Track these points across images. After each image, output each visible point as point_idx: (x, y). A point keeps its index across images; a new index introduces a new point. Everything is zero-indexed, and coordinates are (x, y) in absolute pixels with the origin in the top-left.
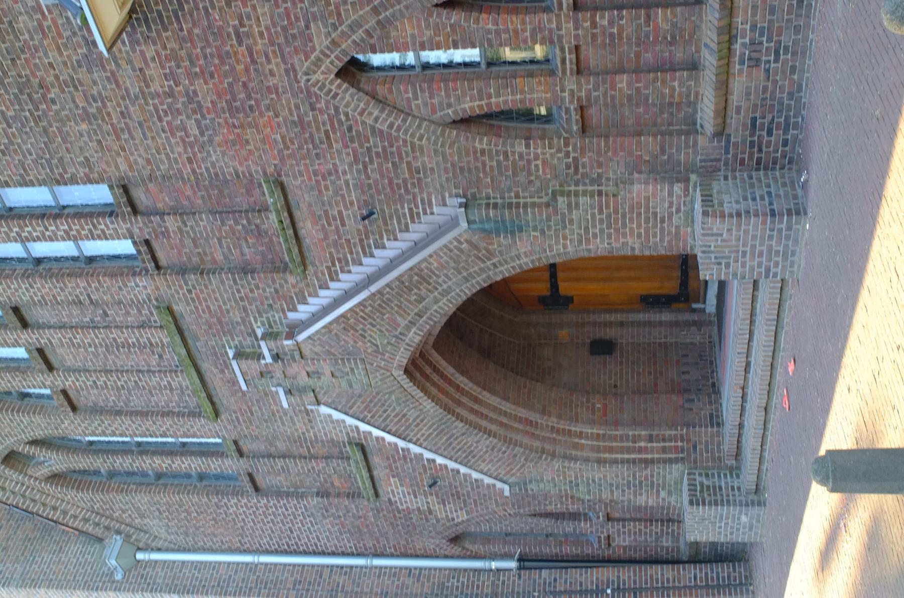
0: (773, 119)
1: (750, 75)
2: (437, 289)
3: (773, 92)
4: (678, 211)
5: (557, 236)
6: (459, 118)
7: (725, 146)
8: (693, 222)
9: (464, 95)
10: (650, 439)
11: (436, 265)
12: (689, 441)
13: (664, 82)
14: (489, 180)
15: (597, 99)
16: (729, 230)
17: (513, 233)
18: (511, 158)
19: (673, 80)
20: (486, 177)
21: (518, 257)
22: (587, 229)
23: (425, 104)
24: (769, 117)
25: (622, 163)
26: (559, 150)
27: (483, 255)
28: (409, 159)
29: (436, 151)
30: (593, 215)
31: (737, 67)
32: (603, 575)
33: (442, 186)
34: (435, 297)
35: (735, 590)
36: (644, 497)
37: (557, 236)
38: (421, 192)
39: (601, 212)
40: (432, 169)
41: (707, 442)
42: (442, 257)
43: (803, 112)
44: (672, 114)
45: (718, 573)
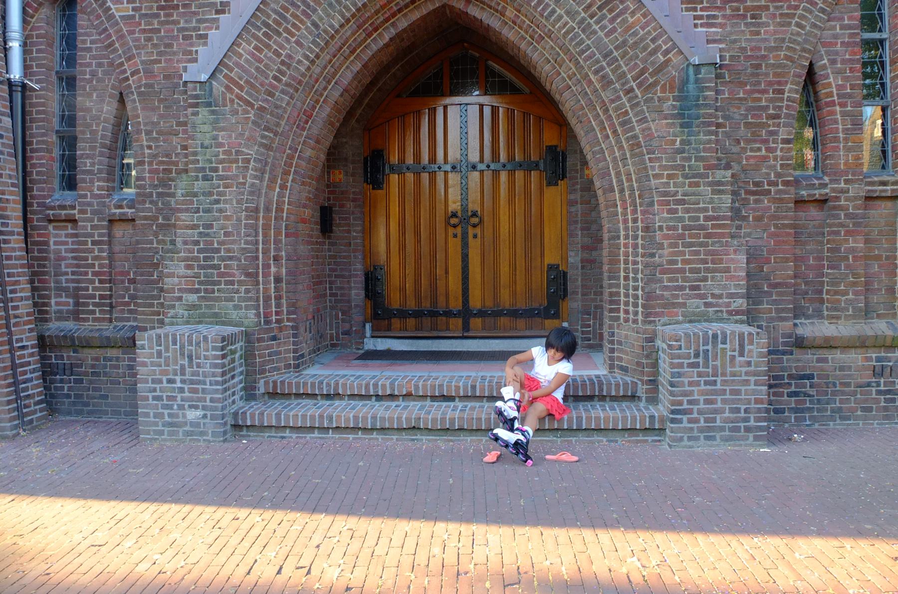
0: (809, 396)
1: (864, 368)
2: (592, 17)
3: (843, 393)
4: (707, 305)
5: (673, 168)
6: (816, 70)
7: (778, 351)
8: (690, 322)
9: (845, 79)
10: (278, 280)
11: (631, 20)
12: (281, 329)
13: (854, 284)
14: (741, 95)
15: (837, 217)
16: (749, 364)
17: (681, 116)
18: (770, 122)
19: (856, 293)
20: (745, 92)
21: (643, 120)
22: (682, 202)
23: (836, 37)
24: (812, 392)
25: (760, 243)
26: (778, 175)
27: (646, 79)
28: (772, 9)
29: (783, 40)
30: (706, 210)
31: (874, 355)
32: (13, 210)
33: (735, 41)
34: (578, 13)
35: (14, 410)
36: (182, 271)
37: (673, 168)
38: (724, 16)
39: (707, 219)
40: (758, 33)
41: (280, 353)
42: (643, 28)
43: (817, 424)
44: (807, 293)
45: (31, 380)
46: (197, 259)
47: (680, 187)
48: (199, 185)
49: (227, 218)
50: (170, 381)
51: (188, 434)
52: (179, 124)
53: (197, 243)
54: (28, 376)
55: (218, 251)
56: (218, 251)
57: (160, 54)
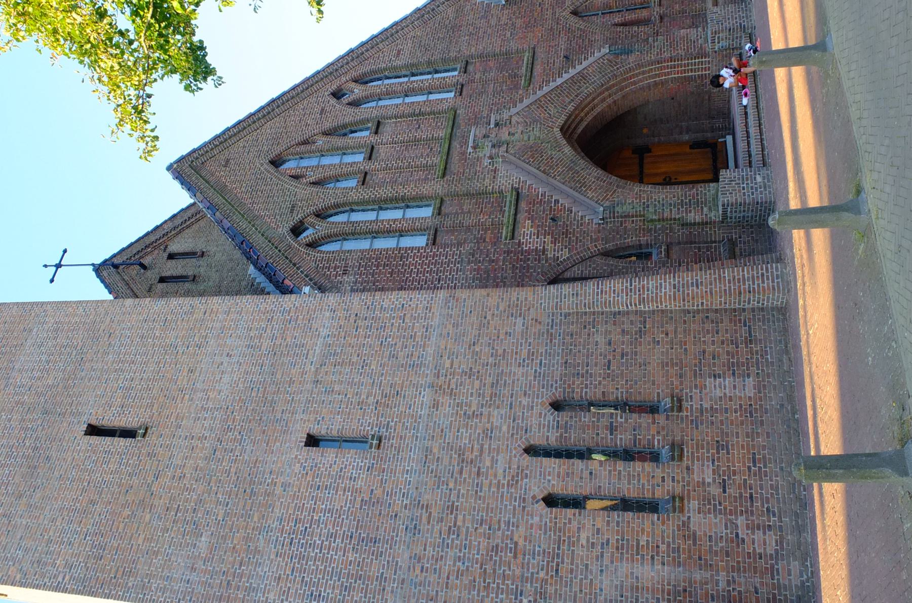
36: (693, 214)
46: (686, 209)
47: (655, 51)
48: (651, 209)
49: (667, 197)
50: (744, 189)
51: (769, 181)
52: (621, 225)
53: (679, 209)
54: (756, 286)
55: (682, 200)
56: (682, 200)
57: (588, 235)
